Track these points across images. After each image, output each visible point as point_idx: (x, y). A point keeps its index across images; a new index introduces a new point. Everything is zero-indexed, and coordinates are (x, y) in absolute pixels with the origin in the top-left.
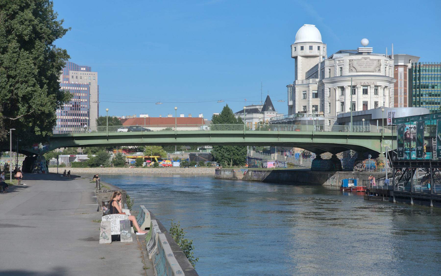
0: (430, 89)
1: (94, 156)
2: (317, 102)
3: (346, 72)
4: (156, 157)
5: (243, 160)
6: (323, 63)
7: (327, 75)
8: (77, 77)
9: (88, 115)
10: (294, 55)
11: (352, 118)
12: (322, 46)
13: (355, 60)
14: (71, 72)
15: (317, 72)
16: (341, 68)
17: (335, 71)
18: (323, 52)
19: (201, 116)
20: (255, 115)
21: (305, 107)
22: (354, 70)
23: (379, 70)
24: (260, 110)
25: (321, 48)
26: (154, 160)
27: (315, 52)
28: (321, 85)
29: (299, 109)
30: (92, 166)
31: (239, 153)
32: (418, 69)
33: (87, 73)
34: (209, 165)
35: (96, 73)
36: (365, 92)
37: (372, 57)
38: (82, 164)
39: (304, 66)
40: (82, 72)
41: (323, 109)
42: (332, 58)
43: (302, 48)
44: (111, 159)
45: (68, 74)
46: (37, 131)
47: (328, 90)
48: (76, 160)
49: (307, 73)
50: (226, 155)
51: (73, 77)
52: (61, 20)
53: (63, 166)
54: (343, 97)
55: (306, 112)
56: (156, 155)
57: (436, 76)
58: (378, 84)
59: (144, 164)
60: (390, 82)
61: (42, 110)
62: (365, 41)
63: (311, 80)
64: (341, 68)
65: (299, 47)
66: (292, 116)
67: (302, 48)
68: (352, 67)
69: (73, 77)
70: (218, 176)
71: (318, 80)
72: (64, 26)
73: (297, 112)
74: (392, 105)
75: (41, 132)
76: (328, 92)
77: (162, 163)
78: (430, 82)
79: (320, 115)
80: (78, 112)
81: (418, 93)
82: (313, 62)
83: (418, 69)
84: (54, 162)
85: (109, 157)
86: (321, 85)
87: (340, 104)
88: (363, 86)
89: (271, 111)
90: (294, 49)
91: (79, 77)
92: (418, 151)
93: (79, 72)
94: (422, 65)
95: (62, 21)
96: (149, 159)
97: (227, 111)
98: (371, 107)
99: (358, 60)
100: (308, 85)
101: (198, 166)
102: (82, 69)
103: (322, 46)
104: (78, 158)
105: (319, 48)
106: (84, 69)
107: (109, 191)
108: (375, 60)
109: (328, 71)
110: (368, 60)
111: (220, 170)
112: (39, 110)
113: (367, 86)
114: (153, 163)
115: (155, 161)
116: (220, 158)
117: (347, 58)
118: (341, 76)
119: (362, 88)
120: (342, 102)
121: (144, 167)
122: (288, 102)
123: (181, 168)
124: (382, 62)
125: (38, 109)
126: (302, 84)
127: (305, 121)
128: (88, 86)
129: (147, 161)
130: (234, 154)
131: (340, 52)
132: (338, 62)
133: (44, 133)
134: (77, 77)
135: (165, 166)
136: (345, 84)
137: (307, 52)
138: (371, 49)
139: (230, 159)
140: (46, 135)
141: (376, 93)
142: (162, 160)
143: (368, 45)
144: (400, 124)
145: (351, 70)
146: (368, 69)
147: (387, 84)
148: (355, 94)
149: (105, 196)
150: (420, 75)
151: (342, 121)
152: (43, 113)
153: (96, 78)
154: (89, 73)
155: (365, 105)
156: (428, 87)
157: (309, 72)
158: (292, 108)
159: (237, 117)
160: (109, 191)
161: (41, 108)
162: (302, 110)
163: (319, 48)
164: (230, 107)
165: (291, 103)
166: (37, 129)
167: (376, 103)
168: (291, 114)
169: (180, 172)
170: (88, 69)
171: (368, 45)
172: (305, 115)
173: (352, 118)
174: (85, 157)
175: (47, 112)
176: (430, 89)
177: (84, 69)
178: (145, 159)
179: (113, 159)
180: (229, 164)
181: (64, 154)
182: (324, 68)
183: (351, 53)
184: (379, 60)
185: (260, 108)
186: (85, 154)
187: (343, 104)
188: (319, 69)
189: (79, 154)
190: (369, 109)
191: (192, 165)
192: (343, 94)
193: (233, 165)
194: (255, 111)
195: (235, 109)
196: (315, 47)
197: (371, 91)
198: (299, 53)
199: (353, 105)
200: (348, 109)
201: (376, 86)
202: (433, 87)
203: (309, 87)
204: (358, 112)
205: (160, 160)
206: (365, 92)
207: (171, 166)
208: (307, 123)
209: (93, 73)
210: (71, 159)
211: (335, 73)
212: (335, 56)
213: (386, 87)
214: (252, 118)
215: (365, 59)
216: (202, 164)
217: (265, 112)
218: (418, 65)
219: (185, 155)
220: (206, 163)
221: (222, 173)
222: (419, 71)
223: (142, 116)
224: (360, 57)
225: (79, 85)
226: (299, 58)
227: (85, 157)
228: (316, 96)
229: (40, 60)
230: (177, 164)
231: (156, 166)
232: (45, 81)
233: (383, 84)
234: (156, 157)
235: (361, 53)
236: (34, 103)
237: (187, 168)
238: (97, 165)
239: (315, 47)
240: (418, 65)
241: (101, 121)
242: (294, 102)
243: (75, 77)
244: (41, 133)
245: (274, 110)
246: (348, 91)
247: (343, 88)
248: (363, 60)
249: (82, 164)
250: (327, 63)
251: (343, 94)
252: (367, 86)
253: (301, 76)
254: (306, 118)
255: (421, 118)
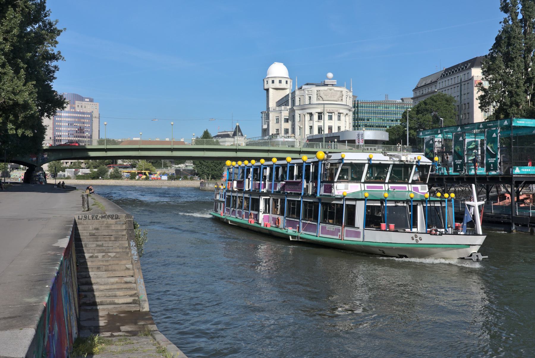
0: (366, 121)
1: (96, 170)
2: (289, 125)
3: (314, 101)
4: (147, 172)
5: (219, 174)
6: (293, 93)
7: (297, 103)
8: (82, 107)
9: (91, 137)
10: (266, 87)
11: (324, 139)
12: (289, 81)
13: (322, 91)
14: (77, 102)
15: (288, 100)
16: (310, 97)
17: (304, 99)
18: (289, 86)
19: (182, 140)
20: (227, 139)
21: (278, 130)
22: (321, 99)
23: (342, 100)
24: (231, 135)
25: (289, 82)
26: (145, 174)
27: (283, 85)
28: (292, 111)
29: (272, 131)
30: (94, 178)
31: (216, 169)
32: (356, 105)
33: (90, 103)
34: (191, 179)
35: (98, 104)
36: (330, 118)
37: (336, 89)
38: (85, 177)
39: (275, 97)
40: (86, 103)
41: (293, 132)
42: (301, 88)
43: (273, 82)
44: (109, 173)
45: (74, 103)
46: (11, 129)
47: (298, 116)
48: (80, 174)
49: (277, 103)
50: (205, 171)
51: (78, 106)
52: (55, 20)
53: (69, 178)
54: (312, 122)
55: (278, 134)
56: (146, 170)
57: (364, 111)
58: (341, 111)
59: (137, 177)
60: (350, 110)
61: (13, 100)
62: (330, 75)
63: (283, 108)
64: (310, 97)
65: (270, 81)
66: (266, 138)
67: (273, 82)
68: (319, 97)
69: (78, 106)
70: (203, 188)
71: (288, 107)
72: (58, 27)
73: (270, 134)
74: (351, 129)
75: (16, 130)
76: (298, 118)
77: (152, 176)
78: (366, 116)
79: (291, 137)
80: (82, 135)
81: (356, 124)
82: (282, 94)
83: (356, 105)
84: (61, 175)
85: (107, 171)
86: (292, 111)
87: (309, 127)
88: (329, 113)
89: (239, 136)
90: (266, 82)
91: (83, 107)
92: (455, 166)
93: (84, 103)
94: (359, 102)
95: (57, 22)
96: (141, 173)
97: (206, 135)
98: (335, 130)
99: (324, 90)
100: (280, 112)
101: (183, 179)
102: (86, 100)
103: (289, 81)
104: (81, 172)
105: (287, 82)
106: (88, 100)
107: (102, 217)
108: (339, 91)
109: (298, 99)
110: (332, 91)
111: (205, 183)
112: (10, 99)
113: (332, 113)
114: (144, 177)
115: (146, 175)
116: (201, 173)
117: (315, 89)
118: (310, 104)
119: (328, 114)
120: (308, 127)
121: (137, 180)
122: (262, 126)
123: (169, 182)
124: (344, 93)
125: (9, 97)
126: (274, 110)
127: (278, 142)
128: (91, 114)
129: (140, 175)
130: (212, 170)
131: (307, 84)
132: (307, 92)
133: (20, 132)
134: (82, 107)
135: (154, 179)
136: (313, 111)
137: (277, 85)
138: (335, 82)
139: (209, 174)
140: (23, 134)
141: (339, 119)
142: (152, 174)
143: (333, 79)
144: (428, 137)
145: (318, 99)
146: (332, 99)
147: (347, 112)
148: (321, 119)
149: (94, 226)
150: (358, 110)
151: (313, 141)
152: (16, 104)
153: (98, 108)
154: (92, 103)
155: (330, 128)
156: (364, 120)
157: (279, 101)
158: (265, 131)
159: (215, 140)
160: (102, 217)
161: (12, 96)
162: (275, 133)
163: (287, 82)
164: (209, 131)
165: (265, 127)
166: (10, 126)
167: (339, 128)
168: (266, 136)
169: (168, 184)
170: (91, 100)
171: (333, 79)
172: (278, 137)
173: (324, 139)
174: (88, 171)
175: (21, 101)
176: (366, 121)
177: (88, 100)
178: (138, 173)
179: (111, 173)
180: (208, 178)
181: (69, 168)
182: (294, 97)
183: (317, 85)
184: (341, 92)
185: (231, 134)
186: (87, 168)
187: (311, 127)
188: (290, 98)
189: (83, 168)
190: (333, 132)
191: (177, 179)
192: (311, 119)
193: (211, 179)
194: (228, 136)
195: (213, 134)
196: (284, 81)
197: (335, 117)
198: (270, 86)
199: (320, 129)
200: (316, 132)
201: (339, 113)
202: (368, 120)
203: (281, 113)
204: (334, 133)
205: (150, 174)
206: (330, 118)
207: (160, 179)
208: (280, 143)
209: (95, 104)
210: (75, 173)
211: (304, 101)
212: (304, 87)
213: (347, 114)
214: (225, 142)
215: (330, 90)
216: (185, 178)
217: (236, 137)
218: (356, 102)
219: (171, 170)
220: (189, 177)
221: (207, 185)
222: (358, 107)
223: (135, 139)
224: (325, 88)
225: (83, 113)
226: (271, 91)
227: (88, 171)
228: (287, 120)
229: (14, 34)
230: (165, 178)
231: (147, 179)
232: (22, 65)
233: (345, 112)
234: (147, 172)
235: (327, 85)
236: (3, 89)
237: (173, 181)
238: (97, 178)
239: (284, 81)
240: (356, 102)
241: (101, 142)
242: (268, 125)
243: (80, 106)
244: (16, 132)
245: (242, 135)
246: (316, 117)
247: (311, 114)
248: (329, 91)
249: (85, 177)
250: (297, 93)
251: (311, 119)
252: (332, 113)
253: (272, 104)
254: (280, 139)
255: (459, 128)
